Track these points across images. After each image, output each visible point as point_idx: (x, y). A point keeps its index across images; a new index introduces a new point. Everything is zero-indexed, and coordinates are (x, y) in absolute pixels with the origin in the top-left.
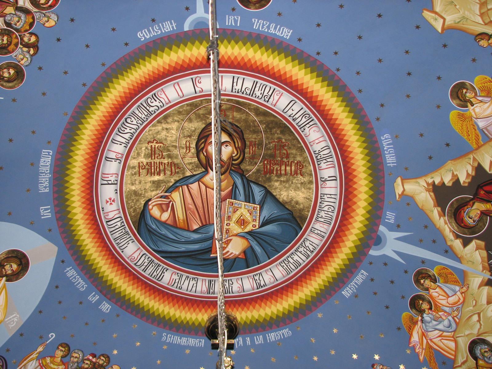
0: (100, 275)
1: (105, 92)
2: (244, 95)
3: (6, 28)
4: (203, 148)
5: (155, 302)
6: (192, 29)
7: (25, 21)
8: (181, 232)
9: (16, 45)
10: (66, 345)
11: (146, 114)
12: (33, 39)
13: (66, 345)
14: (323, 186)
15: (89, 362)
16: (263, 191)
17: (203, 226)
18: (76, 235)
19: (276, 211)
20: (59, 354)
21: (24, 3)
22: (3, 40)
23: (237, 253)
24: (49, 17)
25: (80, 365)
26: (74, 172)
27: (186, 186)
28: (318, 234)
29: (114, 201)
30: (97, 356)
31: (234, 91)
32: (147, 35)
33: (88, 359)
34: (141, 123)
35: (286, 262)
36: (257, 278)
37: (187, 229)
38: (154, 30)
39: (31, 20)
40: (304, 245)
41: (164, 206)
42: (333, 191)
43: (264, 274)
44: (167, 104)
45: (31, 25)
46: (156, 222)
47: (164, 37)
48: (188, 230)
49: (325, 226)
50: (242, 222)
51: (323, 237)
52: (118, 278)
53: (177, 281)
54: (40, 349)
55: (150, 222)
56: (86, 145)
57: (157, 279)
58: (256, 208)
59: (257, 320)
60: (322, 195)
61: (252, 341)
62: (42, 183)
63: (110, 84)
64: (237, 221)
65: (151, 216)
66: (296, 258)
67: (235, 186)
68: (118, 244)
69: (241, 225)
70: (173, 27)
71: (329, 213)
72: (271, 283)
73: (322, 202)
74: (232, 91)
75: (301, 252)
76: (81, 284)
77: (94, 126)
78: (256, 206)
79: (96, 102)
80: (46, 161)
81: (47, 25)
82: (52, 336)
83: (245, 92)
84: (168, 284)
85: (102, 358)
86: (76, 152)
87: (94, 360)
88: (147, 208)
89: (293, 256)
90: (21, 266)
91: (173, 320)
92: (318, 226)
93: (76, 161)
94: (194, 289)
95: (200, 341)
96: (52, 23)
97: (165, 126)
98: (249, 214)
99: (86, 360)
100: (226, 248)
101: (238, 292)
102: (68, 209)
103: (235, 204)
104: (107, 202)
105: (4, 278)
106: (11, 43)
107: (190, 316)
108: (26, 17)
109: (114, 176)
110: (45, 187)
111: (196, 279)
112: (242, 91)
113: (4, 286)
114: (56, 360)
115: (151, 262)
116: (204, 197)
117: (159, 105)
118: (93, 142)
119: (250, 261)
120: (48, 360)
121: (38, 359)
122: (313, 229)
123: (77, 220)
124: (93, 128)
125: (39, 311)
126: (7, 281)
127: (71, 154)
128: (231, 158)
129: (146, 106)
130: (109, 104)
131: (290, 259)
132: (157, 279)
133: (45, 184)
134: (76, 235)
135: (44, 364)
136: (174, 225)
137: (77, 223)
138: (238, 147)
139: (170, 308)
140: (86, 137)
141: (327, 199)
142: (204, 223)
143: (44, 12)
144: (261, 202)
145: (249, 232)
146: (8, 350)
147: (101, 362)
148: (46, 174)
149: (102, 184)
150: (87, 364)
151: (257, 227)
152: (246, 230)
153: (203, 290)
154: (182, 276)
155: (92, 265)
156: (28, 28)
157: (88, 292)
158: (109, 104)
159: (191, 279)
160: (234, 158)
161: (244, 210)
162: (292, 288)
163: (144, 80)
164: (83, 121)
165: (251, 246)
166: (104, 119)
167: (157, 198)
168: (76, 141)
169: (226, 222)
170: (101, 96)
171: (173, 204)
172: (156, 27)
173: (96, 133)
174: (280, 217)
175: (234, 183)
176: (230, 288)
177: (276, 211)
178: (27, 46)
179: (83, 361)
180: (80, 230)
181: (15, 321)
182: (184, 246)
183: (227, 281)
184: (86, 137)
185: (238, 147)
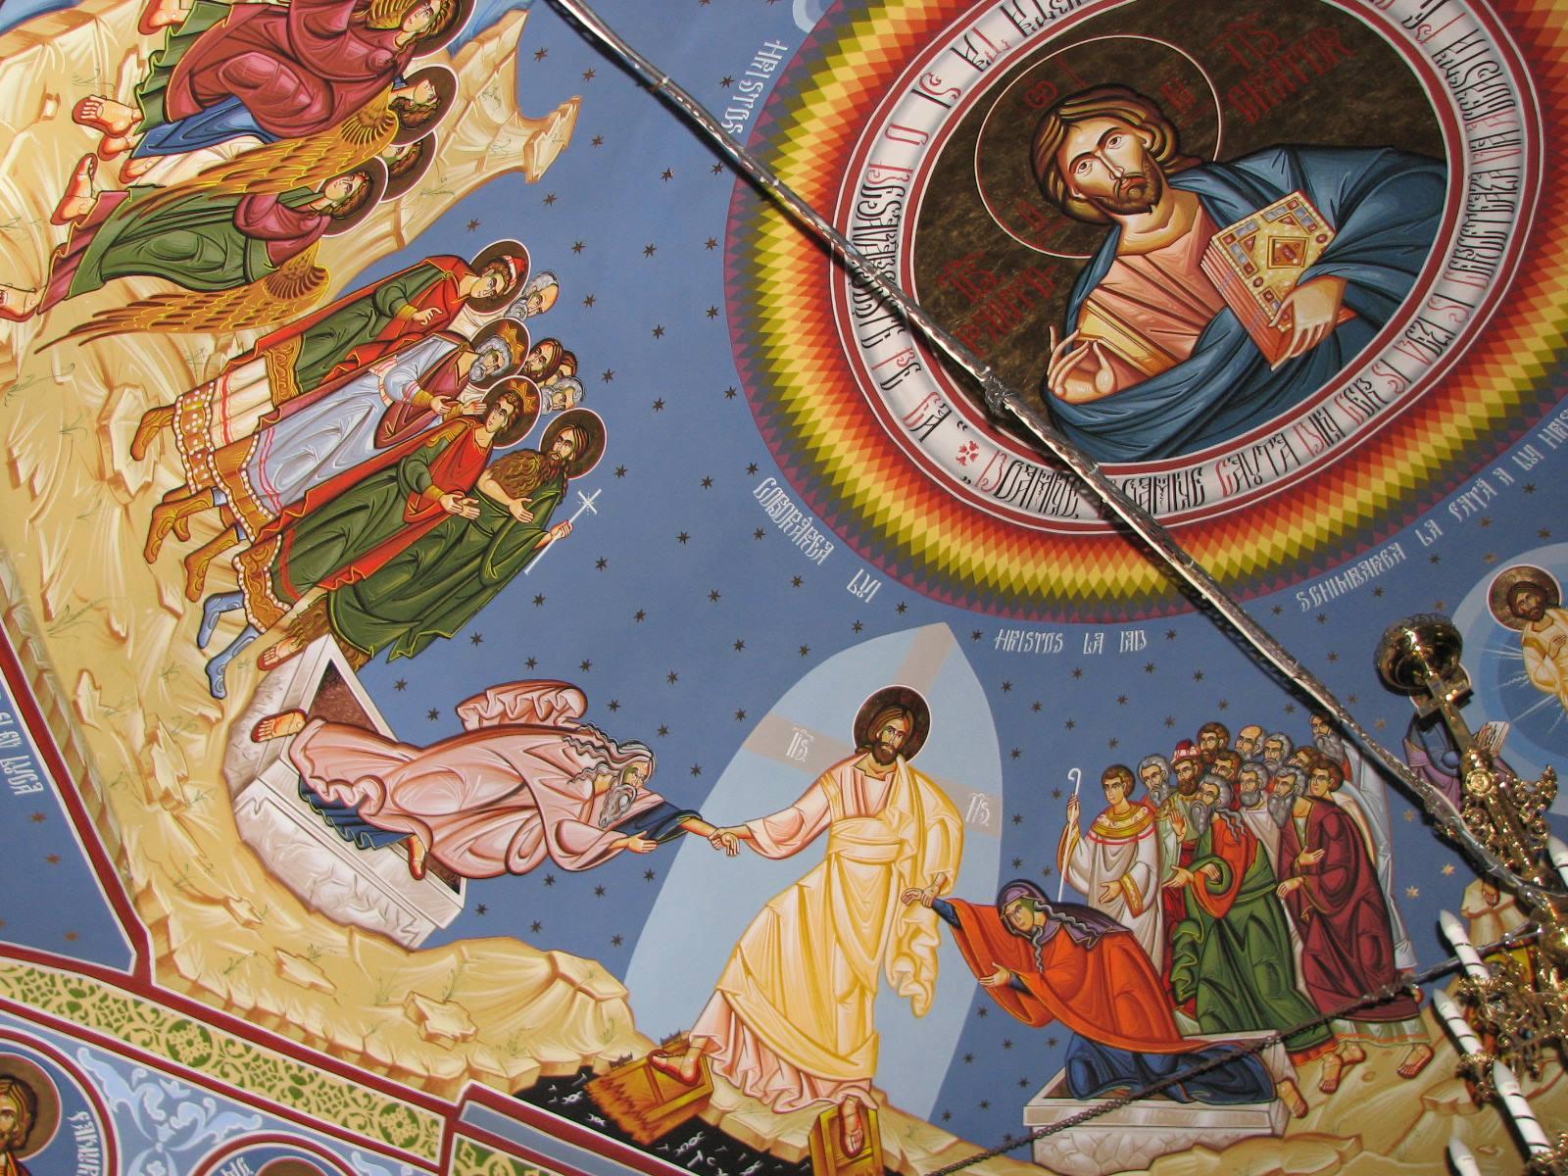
0: (1071, 595)
1: (763, 281)
2: (1061, 18)
3: (487, 391)
4: (1066, 190)
5: (1228, 550)
6: (821, 14)
7: (507, 345)
8: (1165, 381)
9: (532, 391)
10: (1118, 769)
11: (883, 236)
12: (548, 352)
13: (1118, 769)
14: (1423, 37)
15: (1186, 764)
16: (1282, 158)
17: (1204, 331)
18: (958, 571)
19: (1349, 173)
20: (1116, 794)
21: (476, 325)
22: (504, 411)
23: (1329, 318)
24: (536, 293)
25: (1173, 782)
26: (848, 470)
27: (1097, 291)
28: (1496, 145)
29: (973, 447)
30: (1194, 739)
31: (1028, 30)
32: (740, 114)
33: (1181, 760)
34: (889, 260)
35: (1464, 255)
36: (1418, 333)
37: (1172, 363)
38: (745, 95)
39: (513, 332)
40: (1479, 190)
41: (1086, 366)
42: (1460, 29)
43: (1431, 316)
44: (908, 180)
45: (522, 337)
46: (1098, 407)
47: (779, 81)
48: (1179, 363)
49: (1503, 118)
50: (1285, 254)
51: (1518, 141)
52: (1110, 569)
53: (1240, 473)
54: (1073, 815)
55: (1081, 418)
56: (822, 404)
57: (1195, 504)
58: (1295, 200)
59: (1491, 420)
60: (1439, 57)
61: (1513, 469)
62: (809, 545)
63: (758, 260)
64: (1274, 260)
65: (1075, 405)
66: (1481, 229)
67: (1206, 200)
68: (1055, 512)
69: (1289, 259)
70: (778, 52)
71: (1491, 83)
72: (1462, 323)
73: (1452, 72)
74: (1025, 35)
75: (1484, 210)
76: (1049, 641)
77: (802, 356)
78: (1289, 198)
79: (764, 315)
80: (777, 502)
81: (545, 306)
82: (1075, 775)
83: (1056, 12)
84: (1225, 494)
85: (1206, 735)
86: (817, 432)
87: (1193, 752)
88: (1052, 398)
89: (1472, 230)
90: (909, 713)
91: (1295, 554)
92: (1482, 129)
93: (832, 448)
94: (1290, 459)
95: (1390, 553)
96: (549, 294)
97: (945, 220)
98: (1288, 227)
99: (1176, 764)
100: (1293, 328)
101: (1397, 392)
102: (901, 541)
103: (1238, 232)
104: (963, 460)
105: (900, 759)
106: (520, 400)
107: (1327, 519)
108: (500, 339)
109: (930, 402)
110: (822, 546)
111: (1280, 438)
112: (1048, 15)
113: (912, 772)
114: (1118, 809)
115: (1153, 484)
116: (1156, 276)
117: (892, 197)
118: (829, 385)
119: (1374, 312)
120: (1105, 820)
121: (1084, 834)
122: (1476, 144)
123: (936, 545)
124: (806, 362)
125: (1012, 754)
126: (907, 758)
127: (810, 445)
128: (1146, 155)
129: (867, 224)
130: (791, 293)
131: (1468, 242)
132: (1195, 504)
133: (815, 542)
134: (958, 571)
135: (1103, 832)
136: (1139, 380)
137: (941, 550)
138: (1143, 122)
139: (1270, 536)
140: (808, 390)
141: (1459, 58)
142: (1203, 323)
143: (520, 295)
144: (1294, 180)
145: (1320, 258)
146: (1017, 863)
147: (1211, 745)
148: (800, 524)
149: (921, 440)
150: (1185, 769)
151: (1330, 234)
152: (1310, 261)
153: (1312, 446)
154: (1241, 457)
155: (1038, 590)
156: (520, 348)
157: (1074, 644)
158: (791, 293)
159: (1269, 446)
160: (1154, 149)
161: (1269, 227)
162: (1524, 298)
163: (816, 186)
164: (774, 369)
165: (1351, 282)
166: (809, 326)
167: (1056, 362)
168: (796, 415)
169: (1249, 283)
170: (762, 295)
171: (1102, 347)
172: (744, 86)
173: (820, 362)
174: (1369, 177)
175: (1199, 195)
176: (1372, 396)
177: (1349, 173)
178: (548, 372)
179: (1173, 770)
180: (958, 555)
181: (986, 808)
182: (1198, 397)
183: (1354, 389)
184: (808, 390)
185: (1143, 122)
